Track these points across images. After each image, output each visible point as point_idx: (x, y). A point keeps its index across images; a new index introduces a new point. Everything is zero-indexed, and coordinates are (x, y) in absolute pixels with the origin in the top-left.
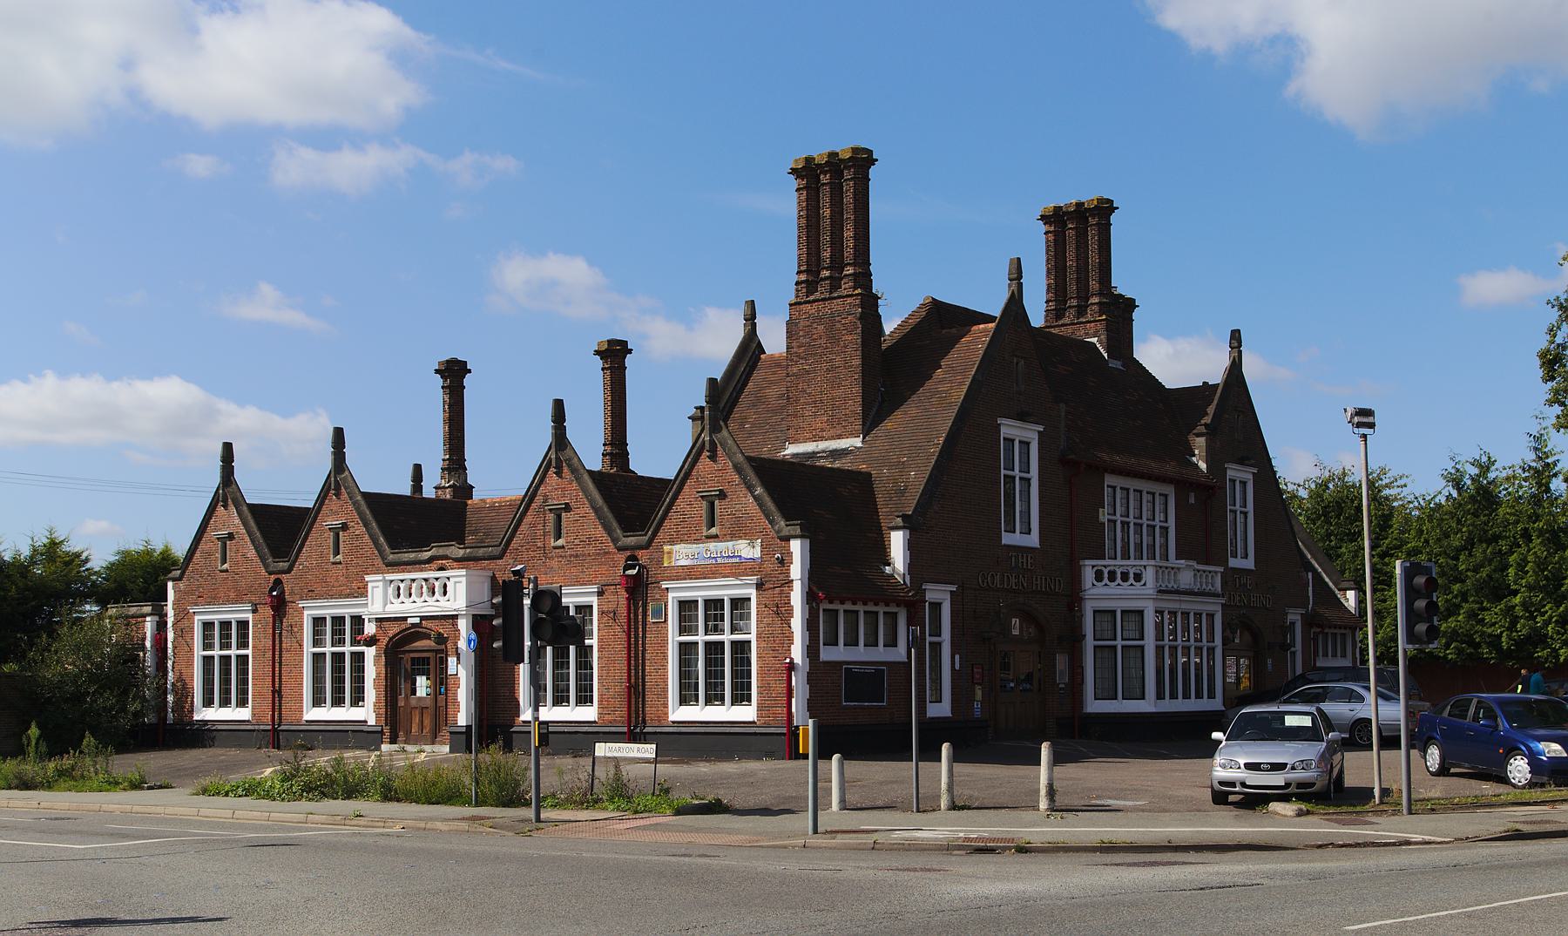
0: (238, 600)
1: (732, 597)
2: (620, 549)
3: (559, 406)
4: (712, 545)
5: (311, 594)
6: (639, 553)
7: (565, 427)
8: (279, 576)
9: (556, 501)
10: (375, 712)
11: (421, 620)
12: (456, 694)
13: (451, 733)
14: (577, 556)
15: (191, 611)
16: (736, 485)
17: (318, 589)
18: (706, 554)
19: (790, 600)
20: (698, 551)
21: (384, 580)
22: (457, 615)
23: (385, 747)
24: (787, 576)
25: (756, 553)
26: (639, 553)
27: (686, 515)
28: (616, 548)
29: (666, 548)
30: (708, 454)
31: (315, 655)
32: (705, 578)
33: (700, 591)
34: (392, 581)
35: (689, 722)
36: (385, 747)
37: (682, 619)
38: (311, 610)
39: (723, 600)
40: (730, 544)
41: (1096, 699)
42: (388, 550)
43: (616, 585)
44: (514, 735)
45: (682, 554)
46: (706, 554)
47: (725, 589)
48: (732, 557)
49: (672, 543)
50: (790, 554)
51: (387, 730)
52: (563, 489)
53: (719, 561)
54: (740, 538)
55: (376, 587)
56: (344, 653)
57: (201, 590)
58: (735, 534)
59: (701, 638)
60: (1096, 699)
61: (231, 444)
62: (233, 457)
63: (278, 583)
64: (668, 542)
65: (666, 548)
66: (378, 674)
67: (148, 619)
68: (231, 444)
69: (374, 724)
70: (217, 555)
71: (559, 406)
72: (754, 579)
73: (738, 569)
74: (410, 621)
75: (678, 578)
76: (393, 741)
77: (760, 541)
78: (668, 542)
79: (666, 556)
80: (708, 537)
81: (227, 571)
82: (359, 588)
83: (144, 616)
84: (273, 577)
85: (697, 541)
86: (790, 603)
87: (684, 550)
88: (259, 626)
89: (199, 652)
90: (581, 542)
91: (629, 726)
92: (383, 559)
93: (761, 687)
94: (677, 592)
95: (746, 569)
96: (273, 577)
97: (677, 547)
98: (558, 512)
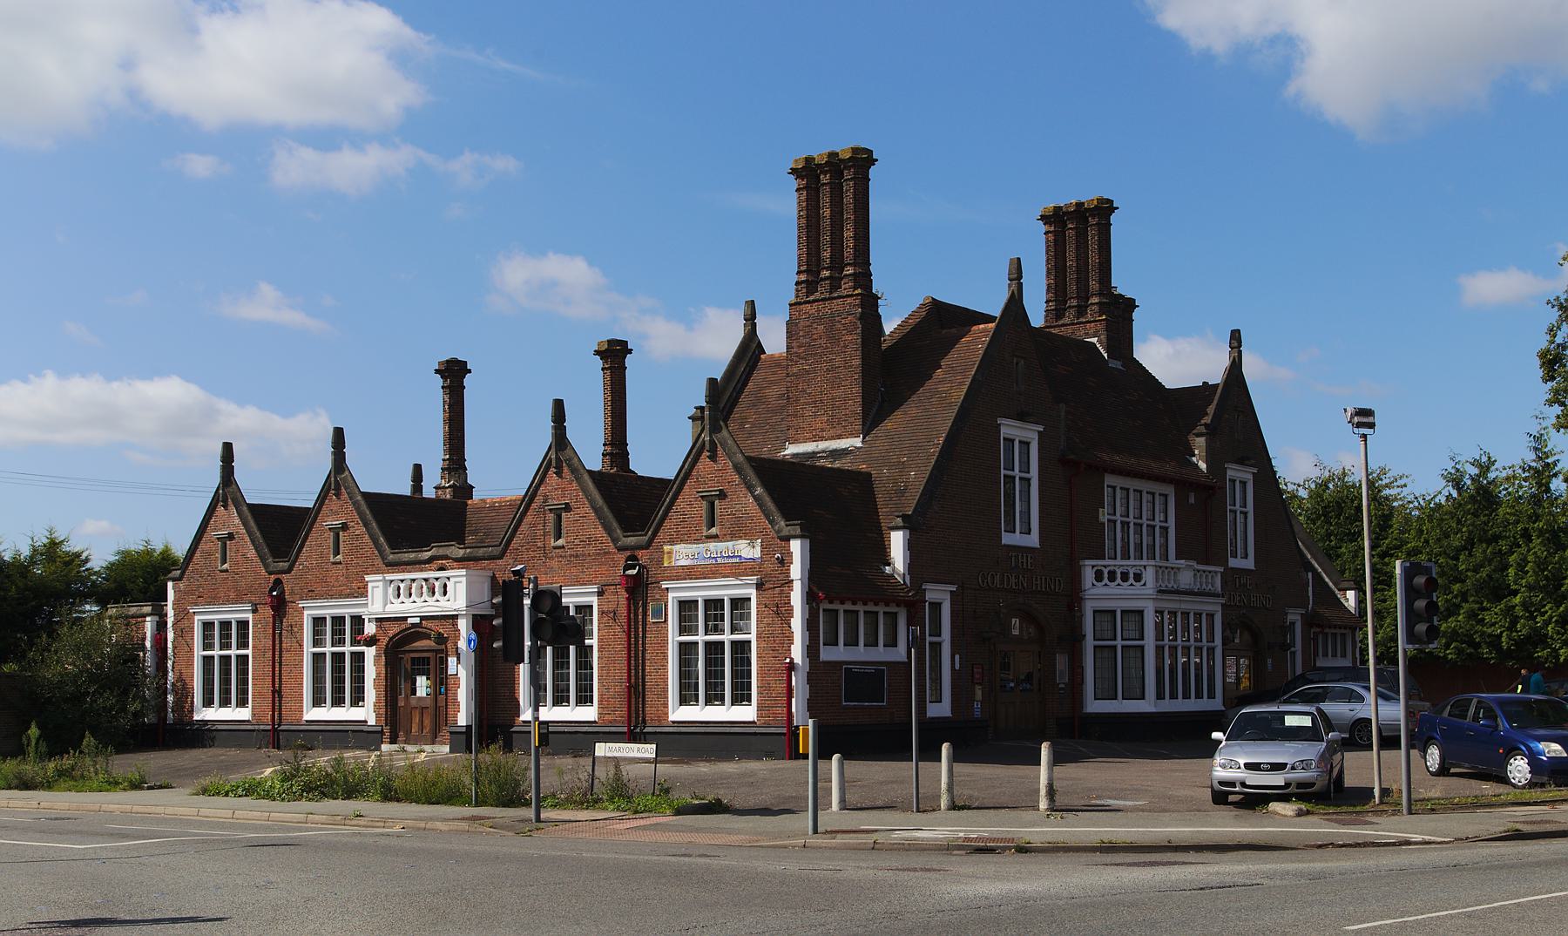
0: (238, 600)
1: (732, 597)
2: (620, 549)
3: (559, 406)
4: (712, 545)
5: (311, 594)
6: (639, 553)
7: (565, 427)
8: (280, 576)
9: (556, 501)
10: (375, 712)
11: (421, 620)
12: (456, 694)
14: (577, 556)
19: (790, 600)
25: (756, 553)
26: (639, 553)
29: (666, 548)
30: (708, 454)
31: (315, 655)
33: (700, 591)
36: (385, 747)
37: (682, 619)
38: (311, 610)
39: (723, 600)
42: (388, 550)
43: (616, 585)
44: (514, 735)
45: (682, 554)
47: (725, 589)
48: (732, 557)
49: (672, 543)
51: (387, 730)
52: (564, 490)
53: (719, 561)
54: (741, 538)
57: (201, 590)
59: (701, 638)
61: (231, 444)
62: (233, 457)
63: (278, 583)
65: (666, 548)
66: (378, 674)
67: (148, 619)
68: (231, 444)
69: (374, 724)
71: (559, 406)
72: (754, 579)
73: (738, 569)
74: (410, 621)
77: (760, 541)
81: (227, 571)
82: (359, 588)
85: (697, 541)
87: (685, 551)
89: (199, 652)
91: (629, 726)
93: (762, 687)
94: (677, 592)
95: (746, 569)
97: (677, 547)
98: (558, 512)
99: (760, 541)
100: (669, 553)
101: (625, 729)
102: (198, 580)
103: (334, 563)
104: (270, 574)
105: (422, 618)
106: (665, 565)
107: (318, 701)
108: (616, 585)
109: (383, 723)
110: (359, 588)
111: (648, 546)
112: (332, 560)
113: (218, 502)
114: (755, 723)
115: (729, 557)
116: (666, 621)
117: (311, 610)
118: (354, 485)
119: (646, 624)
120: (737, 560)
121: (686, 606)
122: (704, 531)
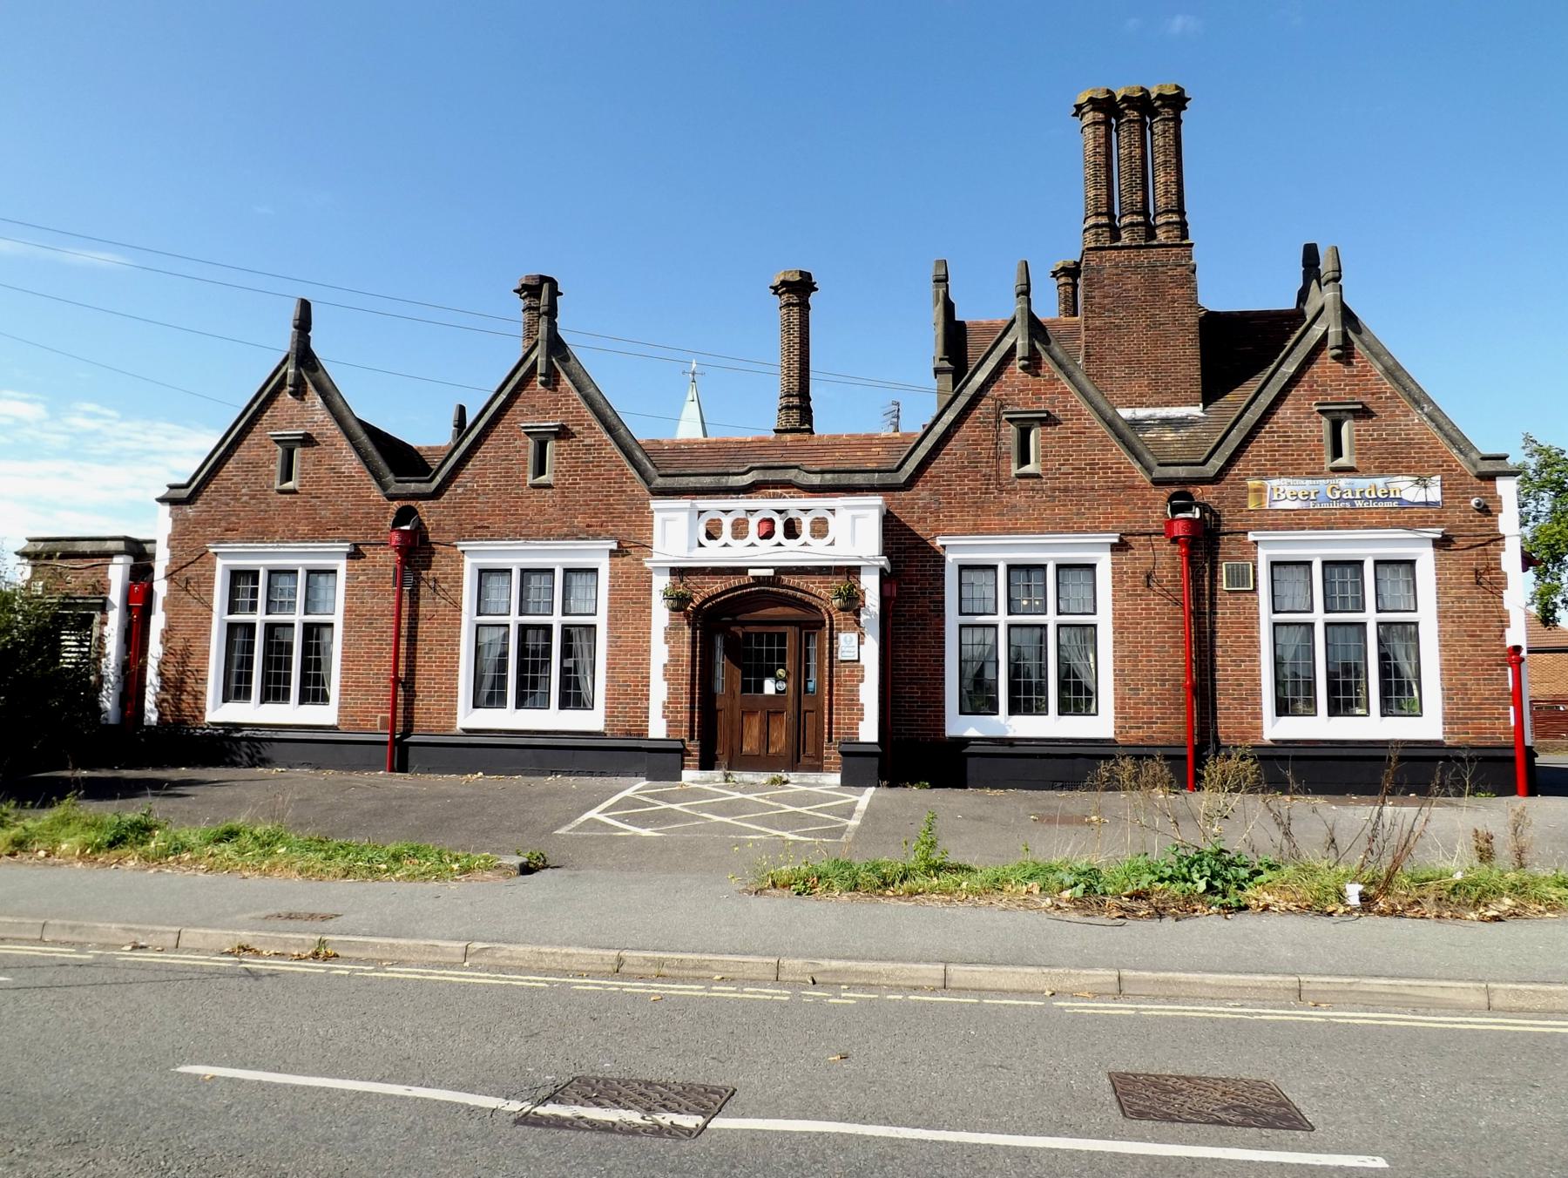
0: (319, 533)
1: (234, 568)
2: (1158, 483)
3: (305, 306)
4: (1343, 482)
5: (481, 531)
6: (422, 506)
7: (309, 338)
8: (412, 503)
9: (1023, 404)
10: (664, 717)
11: (775, 573)
12: (854, 693)
13: (844, 754)
14: (1066, 490)
15: (211, 550)
16: (1387, 398)
17: (497, 523)
18: (1334, 494)
19: (1500, 564)
20: (1316, 488)
21: (690, 510)
22: (859, 568)
23: (690, 776)
24: (1493, 530)
25: (1434, 494)
26: (422, 506)
27: (1289, 436)
28: (385, 495)
29: (1252, 483)
30: (292, 389)
31: (232, 628)
32: (977, 534)
33: (1317, 548)
34: (701, 512)
35: (500, 731)
36: (690, 776)
37: (233, 592)
38: (475, 556)
39: (258, 572)
40: (1380, 482)
41: (961, 713)
42: (390, 477)
43: (1150, 534)
44: (970, 760)
45: (1284, 493)
46: (1334, 494)
47: (1366, 546)
48: (1384, 500)
49: (1263, 475)
50: (1498, 500)
51: (694, 747)
52: (1037, 393)
53: (1359, 504)
54: (1399, 473)
55: (858, 517)
56: (254, 625)
57: (234, 519)
58: (1387, 468)
59: (259, 618)
60: (961, 713)
61: (1315, 245)
62: (310, 323)
63: (405, 515)
64: (1256, 474)
65: (1252, 483)
66: (674, 659)
67: (117, 560)
68: (1315, 245)
69: (664, 737)
70: (272, 467)
71: (305, 306)
72: (346, 547)
73: (1405, 516)
74: (751, 572)
75: (1276, 527)
76: (707, 763)
77: (1438, 478)
78: (1256, 474)
79: (1251, 496)
80: (1337, 470)
81: (294, 492)
82: (588, 526)
83: (109, 555)
84: (396, 505)
85: (1312, 475)
86: (1500, 569)
87: (1287, 488)
88: (361, 578)
89: (219, 617)
90: (1073, 469)
91: (393, 734)
92: (648, 483)
93: (1448, 689)
94: (1269, 548)
95: (1411, 518)
96: (396, 505)
97: (1275, 483)
98: (1026, 424)
99: (1438, 478)
100: (1256, 490)
101: (387, 738)
102: (227, 504)
103: (534, 486)
104: (392, 498)
105: (780, 571)
106: (1250, 508)
107: (236, 689)
108: (1150, 534)
109: (685, 735)
110: (588, 526)
111: (1218, 478)
112: (277, 486)
113: (281, 385)
114: (605, 735)
115: (1377, 499)
116: (1255, 589)
117: (475, 556)
118: (578, 366)
119: (1216, 594)
120: (1395, 504)
121: (241, 579)
122: (277, 482)
